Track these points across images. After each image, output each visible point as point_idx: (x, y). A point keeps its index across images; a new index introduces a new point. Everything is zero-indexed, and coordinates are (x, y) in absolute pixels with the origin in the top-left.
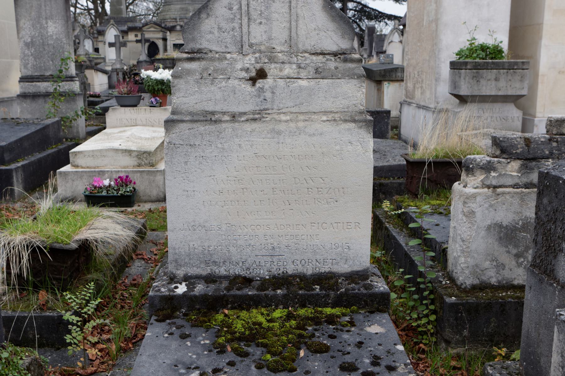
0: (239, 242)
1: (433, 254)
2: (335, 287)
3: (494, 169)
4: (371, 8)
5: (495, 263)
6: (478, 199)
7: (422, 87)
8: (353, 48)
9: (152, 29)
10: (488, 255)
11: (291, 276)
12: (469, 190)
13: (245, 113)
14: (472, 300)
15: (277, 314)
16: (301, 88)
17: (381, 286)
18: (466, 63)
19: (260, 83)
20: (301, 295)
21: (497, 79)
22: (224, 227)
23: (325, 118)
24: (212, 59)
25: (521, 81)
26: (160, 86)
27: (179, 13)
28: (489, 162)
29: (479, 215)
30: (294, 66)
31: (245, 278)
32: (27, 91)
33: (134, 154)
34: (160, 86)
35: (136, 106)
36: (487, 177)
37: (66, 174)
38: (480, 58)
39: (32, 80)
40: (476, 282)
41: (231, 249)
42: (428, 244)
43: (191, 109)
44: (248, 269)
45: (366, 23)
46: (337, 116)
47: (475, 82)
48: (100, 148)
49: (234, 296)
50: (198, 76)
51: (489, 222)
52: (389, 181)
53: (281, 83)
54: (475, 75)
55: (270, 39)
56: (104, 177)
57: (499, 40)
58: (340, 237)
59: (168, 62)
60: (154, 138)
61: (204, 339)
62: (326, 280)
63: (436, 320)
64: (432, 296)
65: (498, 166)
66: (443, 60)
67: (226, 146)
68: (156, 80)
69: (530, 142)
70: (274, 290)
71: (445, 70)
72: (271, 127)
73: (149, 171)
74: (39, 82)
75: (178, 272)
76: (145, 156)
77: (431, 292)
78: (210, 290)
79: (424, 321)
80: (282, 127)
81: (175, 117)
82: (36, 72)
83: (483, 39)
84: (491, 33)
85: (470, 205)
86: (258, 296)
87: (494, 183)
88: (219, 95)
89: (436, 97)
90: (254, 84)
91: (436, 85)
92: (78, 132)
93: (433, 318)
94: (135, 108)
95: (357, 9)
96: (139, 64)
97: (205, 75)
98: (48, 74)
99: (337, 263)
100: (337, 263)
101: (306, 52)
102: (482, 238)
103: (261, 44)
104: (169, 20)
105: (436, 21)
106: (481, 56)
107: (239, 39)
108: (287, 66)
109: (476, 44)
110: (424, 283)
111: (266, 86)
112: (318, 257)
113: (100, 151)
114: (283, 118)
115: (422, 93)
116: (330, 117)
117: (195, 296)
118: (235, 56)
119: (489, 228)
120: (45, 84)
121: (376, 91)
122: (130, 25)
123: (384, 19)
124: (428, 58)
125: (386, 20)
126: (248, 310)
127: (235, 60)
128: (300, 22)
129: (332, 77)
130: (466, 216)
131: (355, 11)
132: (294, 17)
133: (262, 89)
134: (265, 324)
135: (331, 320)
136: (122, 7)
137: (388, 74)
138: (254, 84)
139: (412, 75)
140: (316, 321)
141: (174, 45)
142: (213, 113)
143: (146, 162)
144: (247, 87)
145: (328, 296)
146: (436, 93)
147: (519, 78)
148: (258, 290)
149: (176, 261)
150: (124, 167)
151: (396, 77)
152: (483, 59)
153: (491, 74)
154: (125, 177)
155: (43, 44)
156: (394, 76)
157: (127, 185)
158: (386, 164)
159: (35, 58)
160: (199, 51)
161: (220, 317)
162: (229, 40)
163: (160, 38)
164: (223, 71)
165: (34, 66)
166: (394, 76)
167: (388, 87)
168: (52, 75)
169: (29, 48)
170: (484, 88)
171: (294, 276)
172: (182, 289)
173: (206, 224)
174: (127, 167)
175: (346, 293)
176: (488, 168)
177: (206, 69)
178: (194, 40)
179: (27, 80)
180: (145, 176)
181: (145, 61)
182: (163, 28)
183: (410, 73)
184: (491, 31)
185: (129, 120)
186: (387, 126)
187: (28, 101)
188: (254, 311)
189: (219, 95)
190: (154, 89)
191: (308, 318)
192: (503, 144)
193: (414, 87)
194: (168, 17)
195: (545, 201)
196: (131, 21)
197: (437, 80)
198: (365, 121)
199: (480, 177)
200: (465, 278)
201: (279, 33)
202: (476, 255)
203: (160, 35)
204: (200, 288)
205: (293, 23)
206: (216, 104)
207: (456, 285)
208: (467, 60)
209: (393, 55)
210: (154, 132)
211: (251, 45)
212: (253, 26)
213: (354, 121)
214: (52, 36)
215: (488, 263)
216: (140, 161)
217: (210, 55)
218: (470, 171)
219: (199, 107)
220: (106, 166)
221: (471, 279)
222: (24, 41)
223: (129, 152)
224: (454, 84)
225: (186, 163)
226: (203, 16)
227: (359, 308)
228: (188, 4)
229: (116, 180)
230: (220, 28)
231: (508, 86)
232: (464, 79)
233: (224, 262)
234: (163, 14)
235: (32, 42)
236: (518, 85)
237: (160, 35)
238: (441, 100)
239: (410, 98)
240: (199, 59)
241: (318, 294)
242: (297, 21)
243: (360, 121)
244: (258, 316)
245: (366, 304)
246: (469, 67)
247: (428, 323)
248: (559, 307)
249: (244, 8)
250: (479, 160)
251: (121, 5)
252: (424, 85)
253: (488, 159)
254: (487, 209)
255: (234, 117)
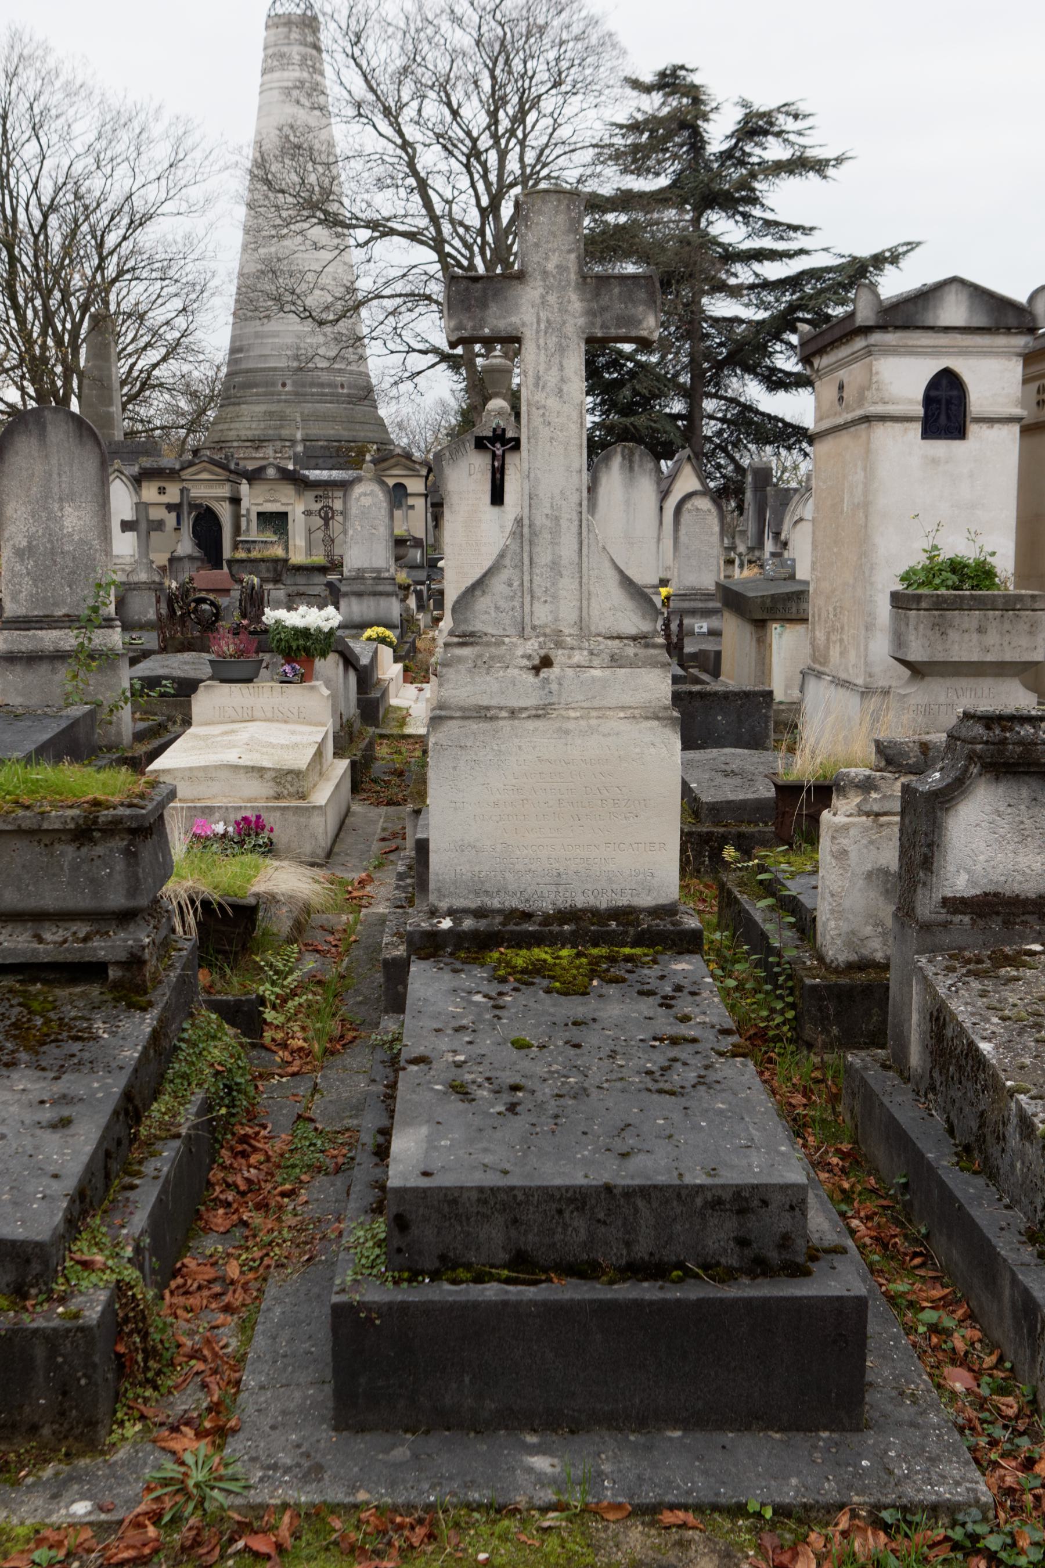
0: (517, 867)
1: (792, 920)
2: (637, 923)
3: (876, 789)
4: (763, 414)
5: (880, 929)
6: (852, 832)
7: (841, 640)
8: (656, 631)
9: (205, 476)
10: (870, 916)
11: (580, 910)
12: (841, 819)
13: (526, 709)
14: (844, 981)
15: (564, 953)
16: (594, 679)
17: (692, 923)
18: (919, 598)
19: (544, 673)
20: (593, 932)
21: (981, 630)
22: (499, 848)
23: (622, 715)
24: (488, 644)
25: (1030, 633)
26: (301, 642)
27: (262, 425)
28: (868, 777)
29: (853, 855)
30: (585, 653)
31: (523, 912)
32: (15, 649)
33: (269, 775)
34: (301, 642)
35: (250, 681)
36: (864, 800)
37: (174, 808)
38: (948, 588)
39: (27, 626)
40: (853, 957)
41: (507, 875)
42: (791, 905)
43: (462, 703)
44: (527, 901)
45: (753, 456)
46: (637, 712)
47: (938, 635)
48: (203, 764)
49: (512, 932)
50: (471, 664)
51: (869, 867)
52: (757, 829)
53: (570, 672)
54: (937, 620)
55: (556, 620)
56: (213, 819)
57: (988, 549)
58: (642, 862)
59: (263, 566)
60: (296, 745)
61: (480, 973)
62: (625, 914)
63: (795, 1018)
64: (790, 984)
65: (882, 783)
66: (880, 586)
67: (503, 748)
68: (295, 629)
69: (928, 749)
70: (561, 925)
71: (883, 609)
72: (558, 725)
73: (297, 807)
74: (41, 629)
75: (441, 904)
76: (289, 778)
77: (789, 977)
78: (482, 924)
79: (779, 1019)
80: (571, 725)
81: (443, 713)
82: (35, 608)
83: (957, 547)
84: (972, 536)
85: (841, 840)
86: (540, 932)
87: (876, 808)
88: (495, 687)
89: (866, 664)
90: (537, 674)
91: (867, 638)
92: (119, 734)
93: (790, 1014)
94: (251, 685)
95: (729, 416)
96: (175, 565)
97: (479, 663)
98: (60, 612)
99: (638, 895)
100: (638, 895)
101: (599, 635)
102: (860, 890)
103: (545, 626)
104: (235, 444)
105: (866, 506)
106: (950, 583)
107: (519, 620)
108: (576, 652)
109: (940, 559)
110: (778, 964)
111: (552, 677)
112: (614, 886)
113: (205, 768)
114: (572, 714)
115: (842, 654)
116: (629, 713)
117: (464, 932)
118: (514, 640)
119: (869, 875)
120: (55, 634)
121: (754, 643)
122: (147, 462)
123: (800, 442)
124: (851, 581)
125: (804, 445)
126: (528, 949)
127: (515, 645)
128: (593, 600)
129: (631, 665)
130: (836, 858)
131: (723, 420)
132: (585, 595)
133: (546, 680)
134: (550, 960)
135: (629, 959)
136: (113, 409)
137: (780, 606)
138: (537, 674)
139: (824, 614)
140: (612, 960)
141: (259, 514)
142: (488, 708)
143: (291, 790)
144: (529, 678)
145: (626, 932)
146: (866, 656)
147: (1026, 627)
148: (540, 925)
149: (439, 890)
150: (249, 801)
151: (798, 612)
152: (955, 589)
153: (972, 619)
154: (254, 819)
155: (53, 551)
156: (794, 610)
157: (257, 834)
158: (750, 796)
159: (34, 580)
160: (472, 634)
161: (496, 955)
162: (507, 622)
163: (223, 499)
164: (500, 658)
165: (32, 596)
166: (794, 610)
167: (780, 635)
168: (68, 616)
169: (23, 560)
170: (956, 647)
171: (584, 911)
172: (446, 924)
173: (478, 844)
174: (256, 800)
175: (649, 930)
176: (866, 786)
177: (480, 656)
178: (466, 621)
179: (17, 625)
180: (290, 816)
181: (190, 558)
182: (231, 472)
183: (820, 609)
184: (972, 531)
185: (239, 710)
186: (766, 722)
187: (18, 668)
188: (536, 950)
189: (495, 687)
190: (290, 647)
191: (602, 957)
192: (888, 751)
193: (828, 640)
194: (232, 434)
195: (907, 822)
196: (147, 453)
197: (869, 627)
198: (671, 718)
199: (855, 800)
200: (836, 951)
201: (568, 613)
202: (850, 917)
203: (225, 491)
204: (468, 924)
205: (585, 602)
206: (492, 697)
207: (825, 963)
208: (920, 591)
209: (794, 560)
210: (293, 733)
211: (534, 628)
212: (536, 604)
213: (657, 718)
214: (70, 535)
215: (870, 928)
216: (279, 789)
217: (485, 639)
218: (842, 791)
219: (473, 701)
220: (214, 797)
221: (846, 953)
222: (14, 546)
223: (259, 771)
224: (899, 640)
225: (455, 768)
226: (478, 593)
227: (665, 949)
228: (286, 401)
229: (237, 823)
230: (497, 608)
231: (1005, 644)
232: (916, 629)
233: (498, 892)
234: (220, 427)
235: (30, 547)
236: (1024, 641)
237: (225, 491)
238: (877, 670)
239: (820, 664)
240: (471, 644)
241: (614, 931)
242: (589, 599)
243: (664, 719)
244: (541, 953)
245: (674, 944)
246: (924, 605)
247: (784, 1023)
248: (917, 953)
249: (526, 584)
250: (853, 774)
251: (110, 403)
252: (845, 637)
253: (868, 772)
254: (866, 847)
255: (513, 713)
